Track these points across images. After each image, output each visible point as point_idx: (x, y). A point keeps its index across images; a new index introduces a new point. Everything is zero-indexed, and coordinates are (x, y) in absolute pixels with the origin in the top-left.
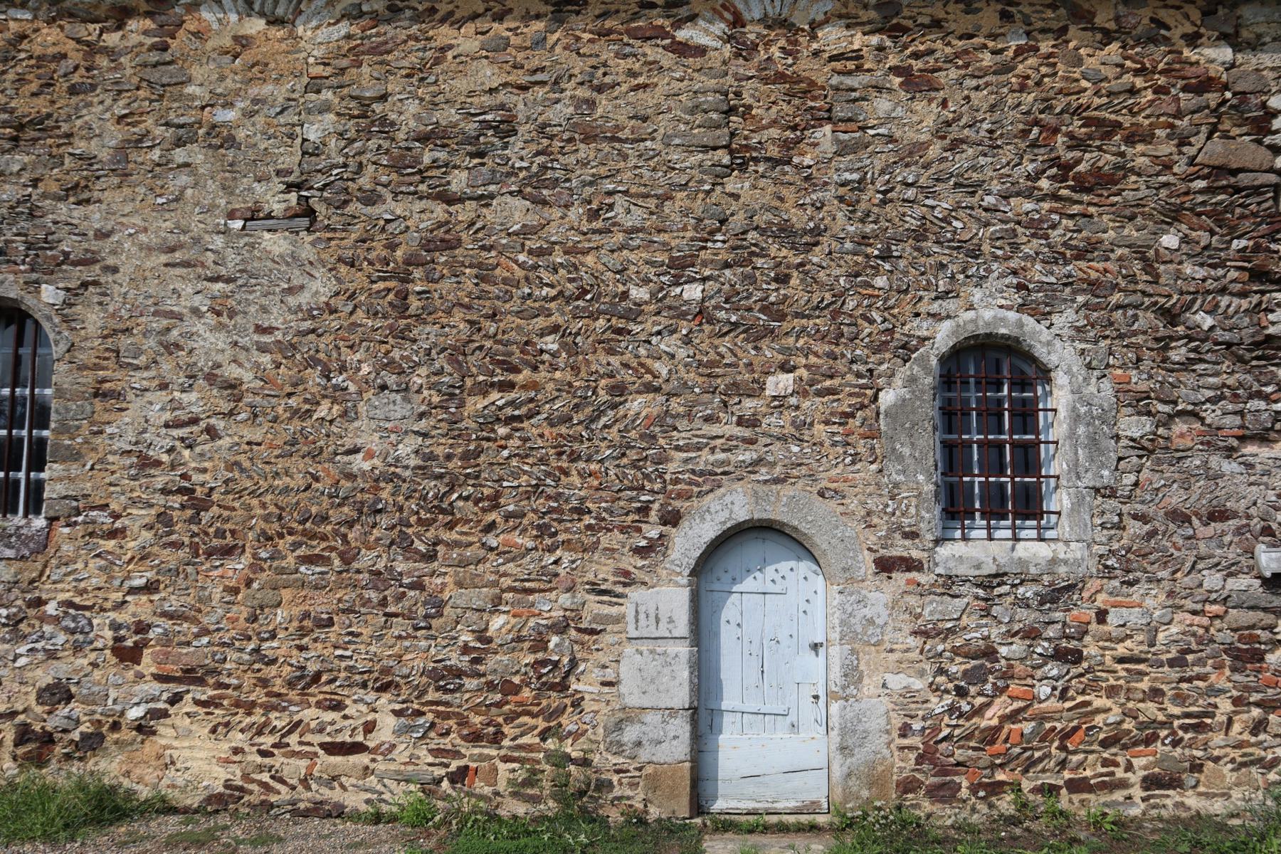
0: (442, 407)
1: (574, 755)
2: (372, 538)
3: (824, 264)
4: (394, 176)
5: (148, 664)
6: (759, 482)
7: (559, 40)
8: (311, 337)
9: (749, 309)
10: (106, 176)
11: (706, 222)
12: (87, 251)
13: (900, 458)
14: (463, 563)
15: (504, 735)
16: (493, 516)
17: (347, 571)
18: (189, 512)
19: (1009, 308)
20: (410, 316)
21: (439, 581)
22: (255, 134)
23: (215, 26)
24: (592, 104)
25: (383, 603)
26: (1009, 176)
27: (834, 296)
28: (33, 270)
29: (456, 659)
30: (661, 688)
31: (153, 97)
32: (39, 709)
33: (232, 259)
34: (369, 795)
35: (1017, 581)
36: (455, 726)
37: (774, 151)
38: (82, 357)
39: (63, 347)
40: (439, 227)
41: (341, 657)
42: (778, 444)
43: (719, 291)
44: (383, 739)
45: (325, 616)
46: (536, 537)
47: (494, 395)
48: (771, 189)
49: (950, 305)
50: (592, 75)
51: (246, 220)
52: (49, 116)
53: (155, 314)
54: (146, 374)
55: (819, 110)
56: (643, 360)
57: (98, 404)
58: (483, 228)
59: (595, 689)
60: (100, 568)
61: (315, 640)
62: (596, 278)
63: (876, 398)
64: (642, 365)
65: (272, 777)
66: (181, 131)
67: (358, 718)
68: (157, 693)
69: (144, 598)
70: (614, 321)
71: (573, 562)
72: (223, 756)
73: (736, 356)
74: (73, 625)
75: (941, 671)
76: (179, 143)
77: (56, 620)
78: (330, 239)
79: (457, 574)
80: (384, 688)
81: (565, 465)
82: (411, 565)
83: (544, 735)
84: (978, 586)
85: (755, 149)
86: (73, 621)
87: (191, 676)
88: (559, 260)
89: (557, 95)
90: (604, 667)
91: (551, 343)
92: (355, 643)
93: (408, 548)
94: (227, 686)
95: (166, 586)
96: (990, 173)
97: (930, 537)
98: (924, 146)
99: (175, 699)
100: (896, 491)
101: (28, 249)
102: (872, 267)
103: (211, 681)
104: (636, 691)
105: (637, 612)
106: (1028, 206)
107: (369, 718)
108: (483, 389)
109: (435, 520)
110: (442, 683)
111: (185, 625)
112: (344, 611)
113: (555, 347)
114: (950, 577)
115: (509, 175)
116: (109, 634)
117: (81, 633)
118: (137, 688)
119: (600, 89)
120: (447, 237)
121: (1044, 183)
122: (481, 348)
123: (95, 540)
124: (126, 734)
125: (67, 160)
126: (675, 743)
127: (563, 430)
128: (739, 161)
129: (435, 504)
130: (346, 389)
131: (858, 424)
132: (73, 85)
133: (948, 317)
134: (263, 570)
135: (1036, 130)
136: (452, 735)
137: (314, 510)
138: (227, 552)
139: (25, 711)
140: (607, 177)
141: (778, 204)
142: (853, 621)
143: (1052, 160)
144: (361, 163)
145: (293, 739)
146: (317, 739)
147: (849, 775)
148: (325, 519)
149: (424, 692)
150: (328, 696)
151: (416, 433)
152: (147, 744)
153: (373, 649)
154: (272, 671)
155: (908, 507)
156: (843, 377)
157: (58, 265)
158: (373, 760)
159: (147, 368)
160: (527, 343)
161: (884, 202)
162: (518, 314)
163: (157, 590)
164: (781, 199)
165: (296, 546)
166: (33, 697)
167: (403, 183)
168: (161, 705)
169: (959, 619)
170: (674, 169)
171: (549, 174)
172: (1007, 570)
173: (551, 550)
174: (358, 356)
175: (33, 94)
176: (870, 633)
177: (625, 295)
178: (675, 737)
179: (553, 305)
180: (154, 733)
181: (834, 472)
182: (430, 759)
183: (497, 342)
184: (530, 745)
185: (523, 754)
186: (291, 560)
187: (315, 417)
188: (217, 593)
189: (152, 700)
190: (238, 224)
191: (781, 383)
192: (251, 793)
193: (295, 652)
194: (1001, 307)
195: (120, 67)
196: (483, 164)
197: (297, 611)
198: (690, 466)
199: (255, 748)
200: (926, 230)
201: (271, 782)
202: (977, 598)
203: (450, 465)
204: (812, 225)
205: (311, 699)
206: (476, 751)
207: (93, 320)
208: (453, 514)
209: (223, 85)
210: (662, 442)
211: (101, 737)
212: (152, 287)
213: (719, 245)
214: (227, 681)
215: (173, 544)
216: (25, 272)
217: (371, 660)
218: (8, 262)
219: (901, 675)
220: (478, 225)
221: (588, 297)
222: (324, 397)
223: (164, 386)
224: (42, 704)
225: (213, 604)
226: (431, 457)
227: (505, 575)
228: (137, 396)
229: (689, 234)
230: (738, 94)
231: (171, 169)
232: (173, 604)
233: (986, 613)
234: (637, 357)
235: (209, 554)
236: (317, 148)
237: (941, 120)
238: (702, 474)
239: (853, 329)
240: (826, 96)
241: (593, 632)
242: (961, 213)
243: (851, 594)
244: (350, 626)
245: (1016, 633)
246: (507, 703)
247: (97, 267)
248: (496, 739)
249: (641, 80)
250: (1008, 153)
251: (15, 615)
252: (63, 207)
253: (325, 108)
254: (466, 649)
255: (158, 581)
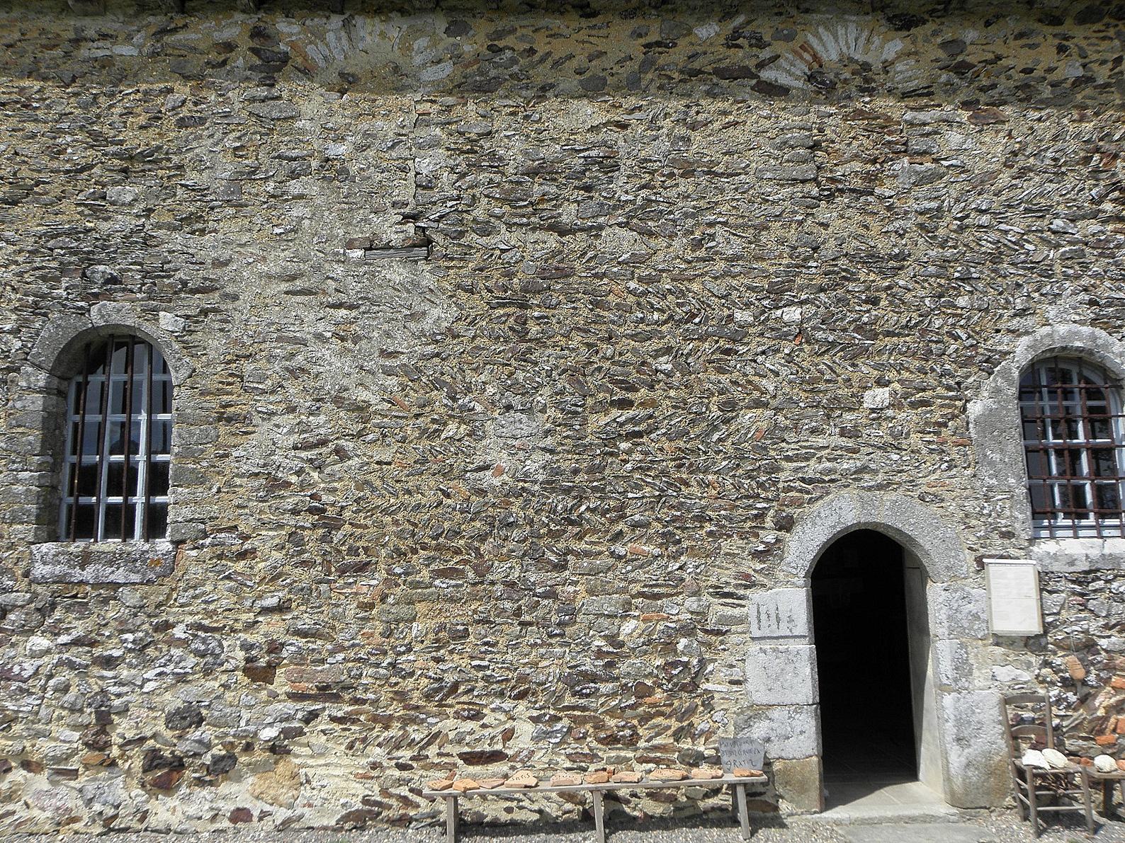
0: (565, 425)
1: (707, 753)
2: (505, 550)
3: (910, 287)
4: (506, 208)
5: (281, 684)
6: (863, 488)
7: (652, 80)
8: (436, 360)
9: (844, 330)
10: (221, 206)
11: (800, 250)
12: (205, 279)
13: (992, 463)
14: (594, 572)
15: (640, 737)
16: (621, 526)
17: (482, 583)
18: (321, 531)
19: (1082, 323)
20: (530, 340)
21: (571, 589)
22: (369, 167)
23: (321, 64)
24: (687, 140)
25: (518, 613)
26: (1075, 200)
27: (920, 316)
28: (150, 299)
29: (589, 664)
30: (786, 685)
31: (263, 130)
32: (168, 734)
33: (353, 286)
34: (508, 804)
35: (1110, 577)
36: (591, 730)
37: (857, 183)
38: (202, 383)
39: (184, 373)
40: (553, 257)
41: (479, 668)
42: (880, 453)
43: (816, 314)
44: (521, 746)
45: (460, 628)
46: (662, 544)
47: (615, 412)
48: (858, 218)
49: (1029, 321)
50: (686, 114)
51: (366, 249)
52: (159, 148)
53: (279, 339)
54: (272, 398)
55: (897, 144)
56: (751, 378)
57: (223, 429)
58: (595, 256)
59: (724, 688)
60: (230, 590)
61: (451, 652)
62: (703, 302)
63: (964, 409)
64: (750, 382)
65: (411, 790)
66: (294, 164)
67: (497, 726)
68: (292, 712)
69: (276, 617)
70: (722, 343)
71: (697, 567)
72: (360, 771)
73: (835, 372)
74: (203, 648)
75: (1047, 664)
76: (294, 175)
77: (184, 643)
78: (448, 268)
79: (588, 581)
80: (521, 696)
81: (684, 476)
82: (543, 574)
83: (678, 736)
84: (1073, 582)
85: (840, 181)
86: (204, 643)
87: (326, 693)
88: (668, 287)
89: (654, 133)
90: (732, 666)
91: (664, 363)
92: (491, 652)
93: (539, 560)
94: (364, 702)
95: (298, 605)
96: (1056, 198)
97: (1024, 536)
98: (993, 175)
99: (311, 717)
100: (991, 494)
101: (144, 277)
102: (954, 288)
103: (347, 697)
104: (763, 688)
105: (758, 612)
106: (1094, 227)
107: (507, 726)
108: (602, 407)
109: (565, 532)
110: (577, 688)
111: (319, 642)
112: (478, 622)
113: (669, 367)
114: (1047, 573)
115: (615, 208)
116: (241, 655)
117: (212, 654)
118: (270, 708)
119: (693, 127)
120: (561, 265)
121: (1108, 206)
122: (599, 369)
123: (224, 562)
124: (259, 755)
125: (179, 191)
126: (801, 737)
127: (682, 445)
128: (826, 193)
129: (567, 513)
130: (473, 409)
131: (950, 433)
132: (182, 119)
133: (1027, 333)
134: (397, 585)
135: (1097, 157)
136: (589, 739)
137: (446, 525)
138: (362, 568)
139: (154, 736)
140: (707, 208)
141: (863, 231)
142: (960, 616)
143: (1114, 184)
144: (474, 196)
145: (432, 751)
146: (456, 750)
147: (968, 765)
148: (457, 534)
149: (560, 698)
150: (466, 707)
151: (543, 449)
152: (282, 763)
153: (509, 657)
154: (409, 683)
155: (1003, 508)
156: (934, 389)
157: (176, 293)
158: (513, 768)
159: (273, 392)
160: (643, 363)
161: (961, 229)
162: (632, 337)
163: (289, 609)
164: (867, 227)
165: (431, 560)
166: (162, 722)
167: (516, 215)
168: (296, 724)
169: (1058, 613)
170: (768, 201)
171: (654, 207)
172: (1099, 566)
173: (675, 557)
174: (483, 378)
175: (142, 127)
176: (975, 627)
177: (730, 318)
178: (802, 732)
179: (664, 328)
180: (288, 752)
181: (933, 477)
182: (568, 764)
183: (613, 363)
184: (664, 746)
185: (659, 754)
186: (425, 575)
187: (443, 436)
188: (352, 610)
189: (287, 720)
190: (357, 254)
191: (877, 397)
192: (390, 807)
193: (432, 664)
194: (1075, 322)
195: (227, 101)
196: (591, 198)
197: (432, 624)
198: (800, 475)
199: (394, 762)
200: (1001, 253)
201: (410, 795)
202: (1074, 593)
203: (577, 479)
204: (897, 251)
205: (448, 710)
206: (613, 754)
207: (215, 344)
208: (581, 525)
209: (333, 119)
210: (772, 453)
211: (232, 758)
212: (274, 314)
213: (814, 270)
214: (364, 696)
215: (304, 563)
216: (142, 299)
217: (508, 668)
218: (124, 290)
219: (1009, 667)
220: (590, 254)
221: (697, 320)
222: (451, 416)
223: (291, 410)
224: (171, 729)
225: (348, 620)
226: (558, 472)
227: (634, 581)
228: (263, 420)
229: (785, 262)
230: (821, 130)
231: (287, 200)
232: (306, 622)
233: (1083, 607)
234: (745, 375)
235: (342, 572)
236: (430, 182)
237: (1008, 150)
238: (810, 481)
239: (940, 346)
240: (902, 131)
241: (719, 633)
242: (1031, 237)
243: (956, 591)
244: (486, 637)
245: (1114, 626)
246: (641, 705)
247: (217, 294)
248: (632, 742)
249: (731, 118)
250: (1070, 180)
251: (141, 639)
252: (178, 237)
253: (434, 144)
254: (600, 654)
255: (290, 600)
